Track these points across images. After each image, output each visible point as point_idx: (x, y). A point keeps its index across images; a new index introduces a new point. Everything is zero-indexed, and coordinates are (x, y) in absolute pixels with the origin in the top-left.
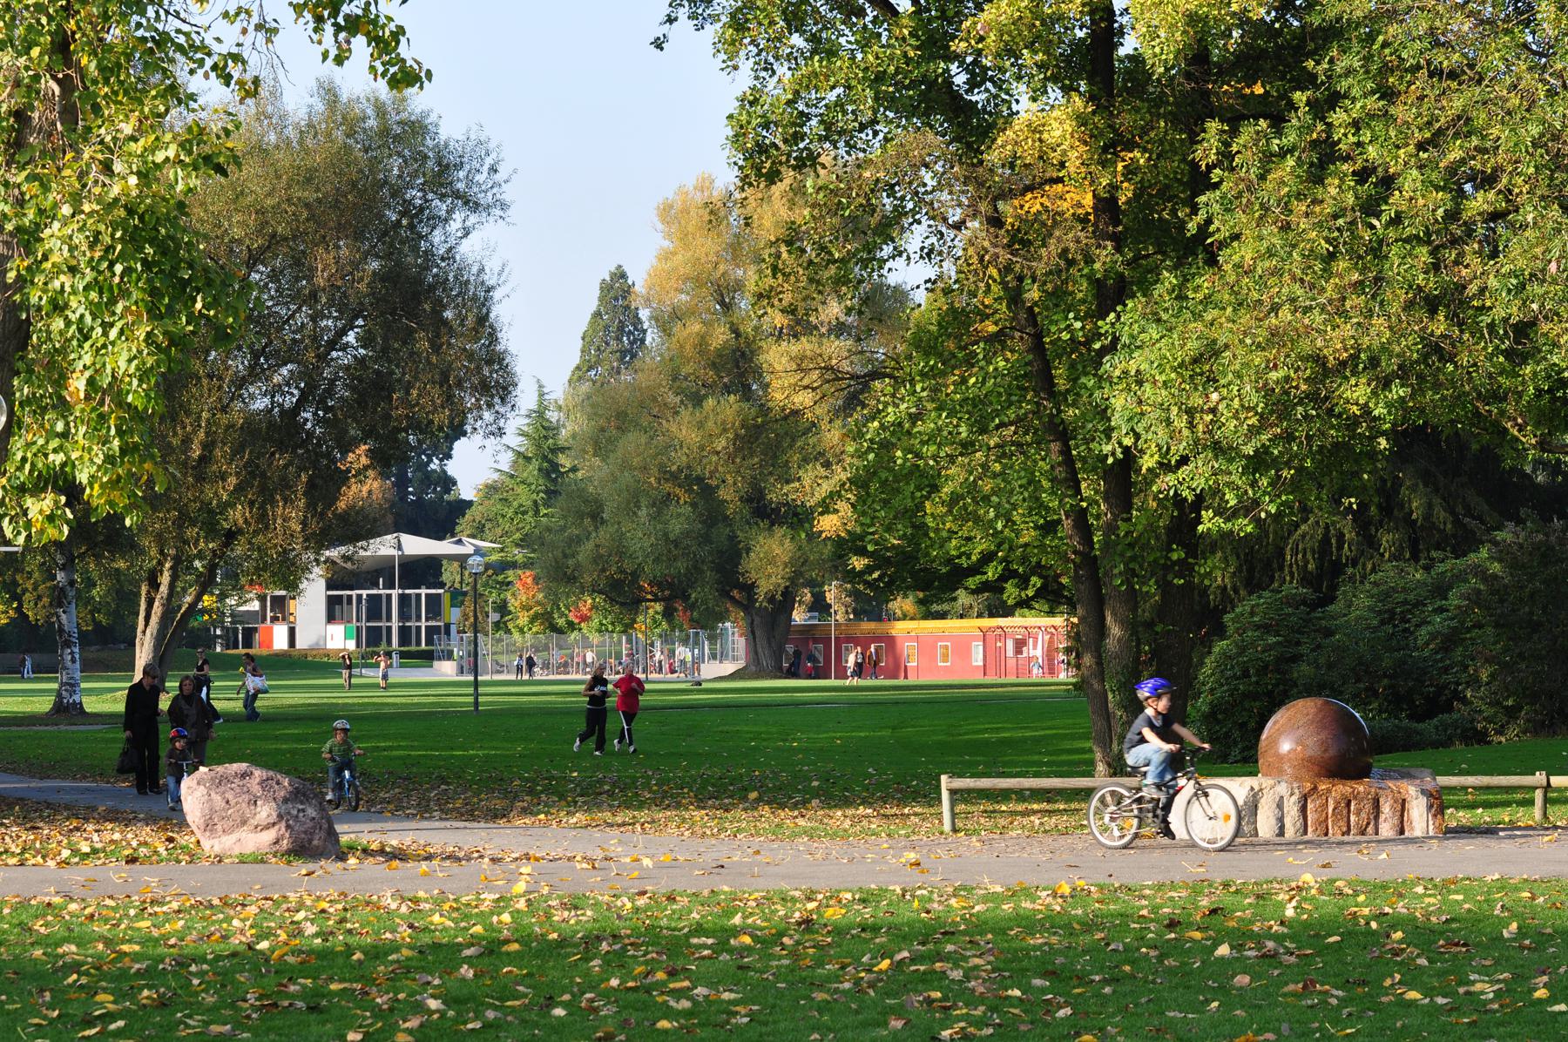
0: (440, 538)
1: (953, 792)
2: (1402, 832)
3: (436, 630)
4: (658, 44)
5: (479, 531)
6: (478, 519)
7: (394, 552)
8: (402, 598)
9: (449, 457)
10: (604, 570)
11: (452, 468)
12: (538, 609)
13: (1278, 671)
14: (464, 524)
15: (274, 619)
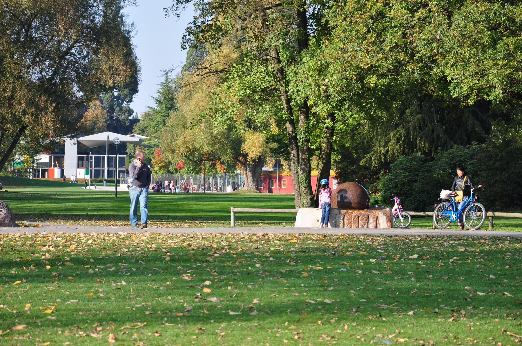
0: (126, 134)
2: (376, 227)
3: (123, 172)
5: (142, 131)
6: (141, 127)
7: (106, 139)
8: (108, 158)
9: (131, 101)
10: (187, 147)
11: (132, 106)
12: (163, 164)
13: (409, 185)
14: (136, 128)
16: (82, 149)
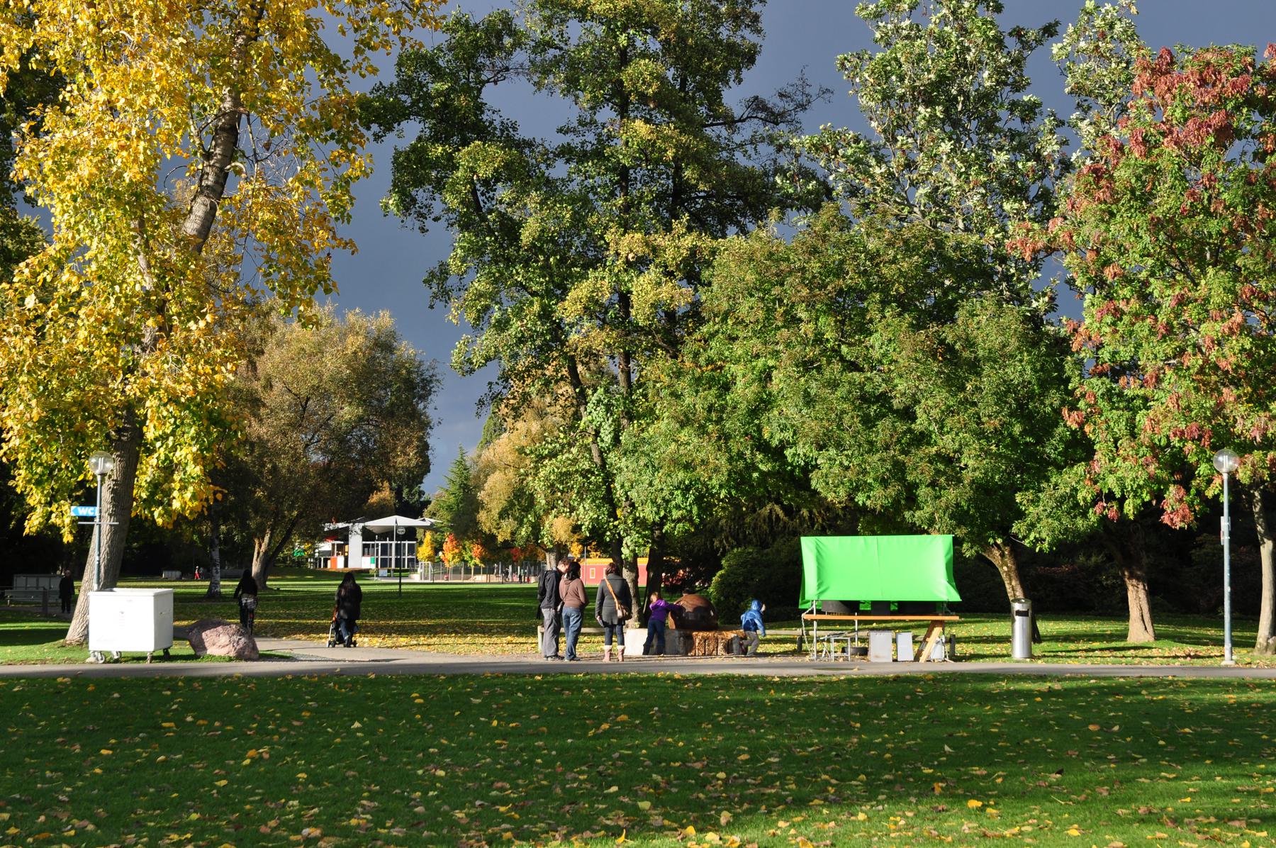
4: (432, 307)
5: (433, 515)
11: (423, 487)
16: (367, 535)
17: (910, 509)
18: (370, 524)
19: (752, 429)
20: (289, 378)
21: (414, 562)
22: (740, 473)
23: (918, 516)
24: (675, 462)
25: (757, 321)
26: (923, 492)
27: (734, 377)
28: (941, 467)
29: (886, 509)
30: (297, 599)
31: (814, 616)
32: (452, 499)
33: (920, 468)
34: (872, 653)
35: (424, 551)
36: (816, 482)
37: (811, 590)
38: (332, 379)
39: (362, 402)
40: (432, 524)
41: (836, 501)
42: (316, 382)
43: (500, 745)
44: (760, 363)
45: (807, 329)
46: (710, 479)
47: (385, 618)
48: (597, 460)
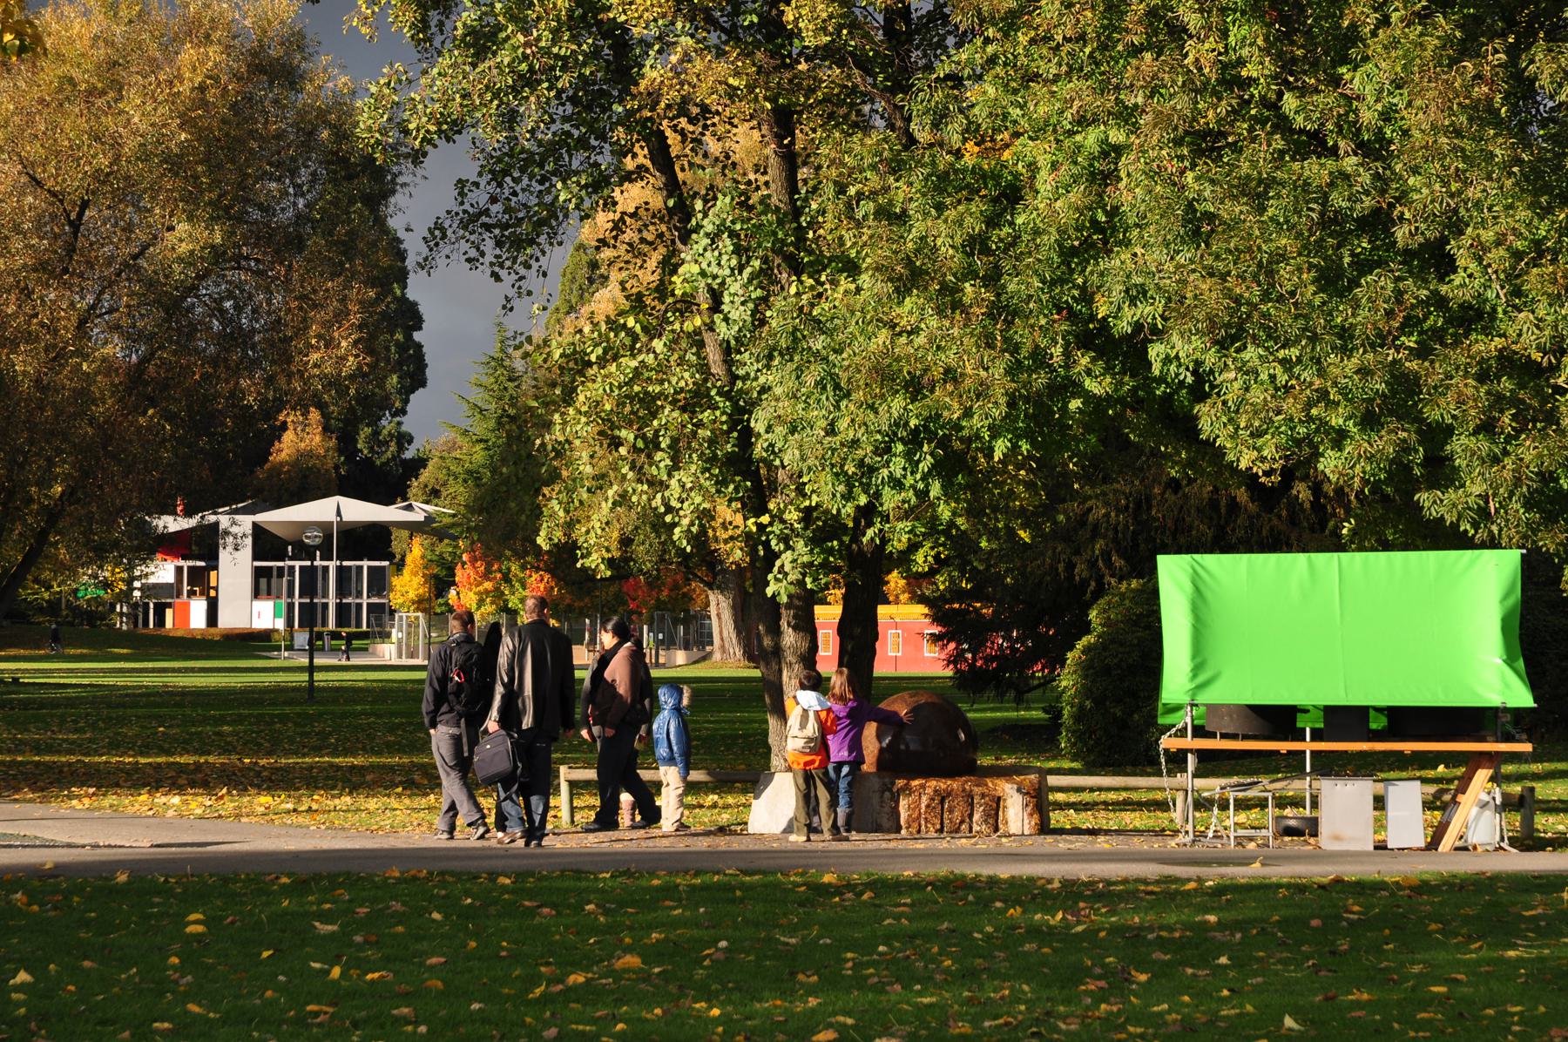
1: (573, 784)
5: (433, 494)
8: (340, 569)
11: (409, 424)
15: (191, 593)
16: (266, 544)
17: (1431, 486)
18: (268, 517)
19: (1069, 295)
20: (33, 151)
21: (383, 614)
22: (1036, 400)
23: (1433, 503)
24: (886, 375)
25: (1082, 38)
26: (1461, 446)
27: (1033, 167)
28: (1506, 385)
29: (1376, 487)
30: (54, 704)
31: (1189, 742)
32: (479, 455)
33: (1454, 395)
34: (1324, 828)
35: (408, 585)
36: (1209, 419)
37: (1175, 683)
38: (144, 155)
39: (221, 212)
40: (430, 519)
41: (1259, 469)
42: (103, 161)
43: (316, 1014)
44: (1090, 139)
45: (1201, 53)
46: (968, 413)
47: (258, 751)
48: (717, 369)
